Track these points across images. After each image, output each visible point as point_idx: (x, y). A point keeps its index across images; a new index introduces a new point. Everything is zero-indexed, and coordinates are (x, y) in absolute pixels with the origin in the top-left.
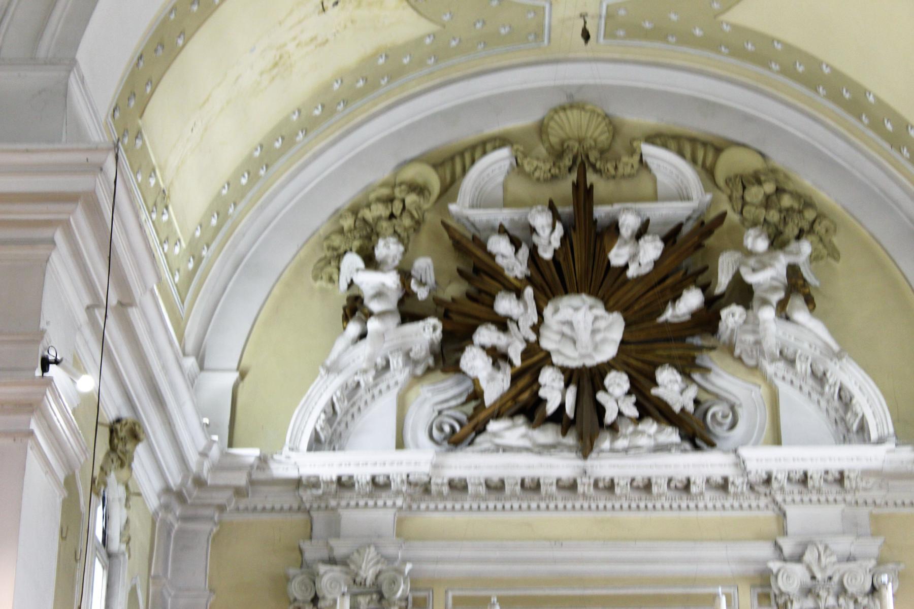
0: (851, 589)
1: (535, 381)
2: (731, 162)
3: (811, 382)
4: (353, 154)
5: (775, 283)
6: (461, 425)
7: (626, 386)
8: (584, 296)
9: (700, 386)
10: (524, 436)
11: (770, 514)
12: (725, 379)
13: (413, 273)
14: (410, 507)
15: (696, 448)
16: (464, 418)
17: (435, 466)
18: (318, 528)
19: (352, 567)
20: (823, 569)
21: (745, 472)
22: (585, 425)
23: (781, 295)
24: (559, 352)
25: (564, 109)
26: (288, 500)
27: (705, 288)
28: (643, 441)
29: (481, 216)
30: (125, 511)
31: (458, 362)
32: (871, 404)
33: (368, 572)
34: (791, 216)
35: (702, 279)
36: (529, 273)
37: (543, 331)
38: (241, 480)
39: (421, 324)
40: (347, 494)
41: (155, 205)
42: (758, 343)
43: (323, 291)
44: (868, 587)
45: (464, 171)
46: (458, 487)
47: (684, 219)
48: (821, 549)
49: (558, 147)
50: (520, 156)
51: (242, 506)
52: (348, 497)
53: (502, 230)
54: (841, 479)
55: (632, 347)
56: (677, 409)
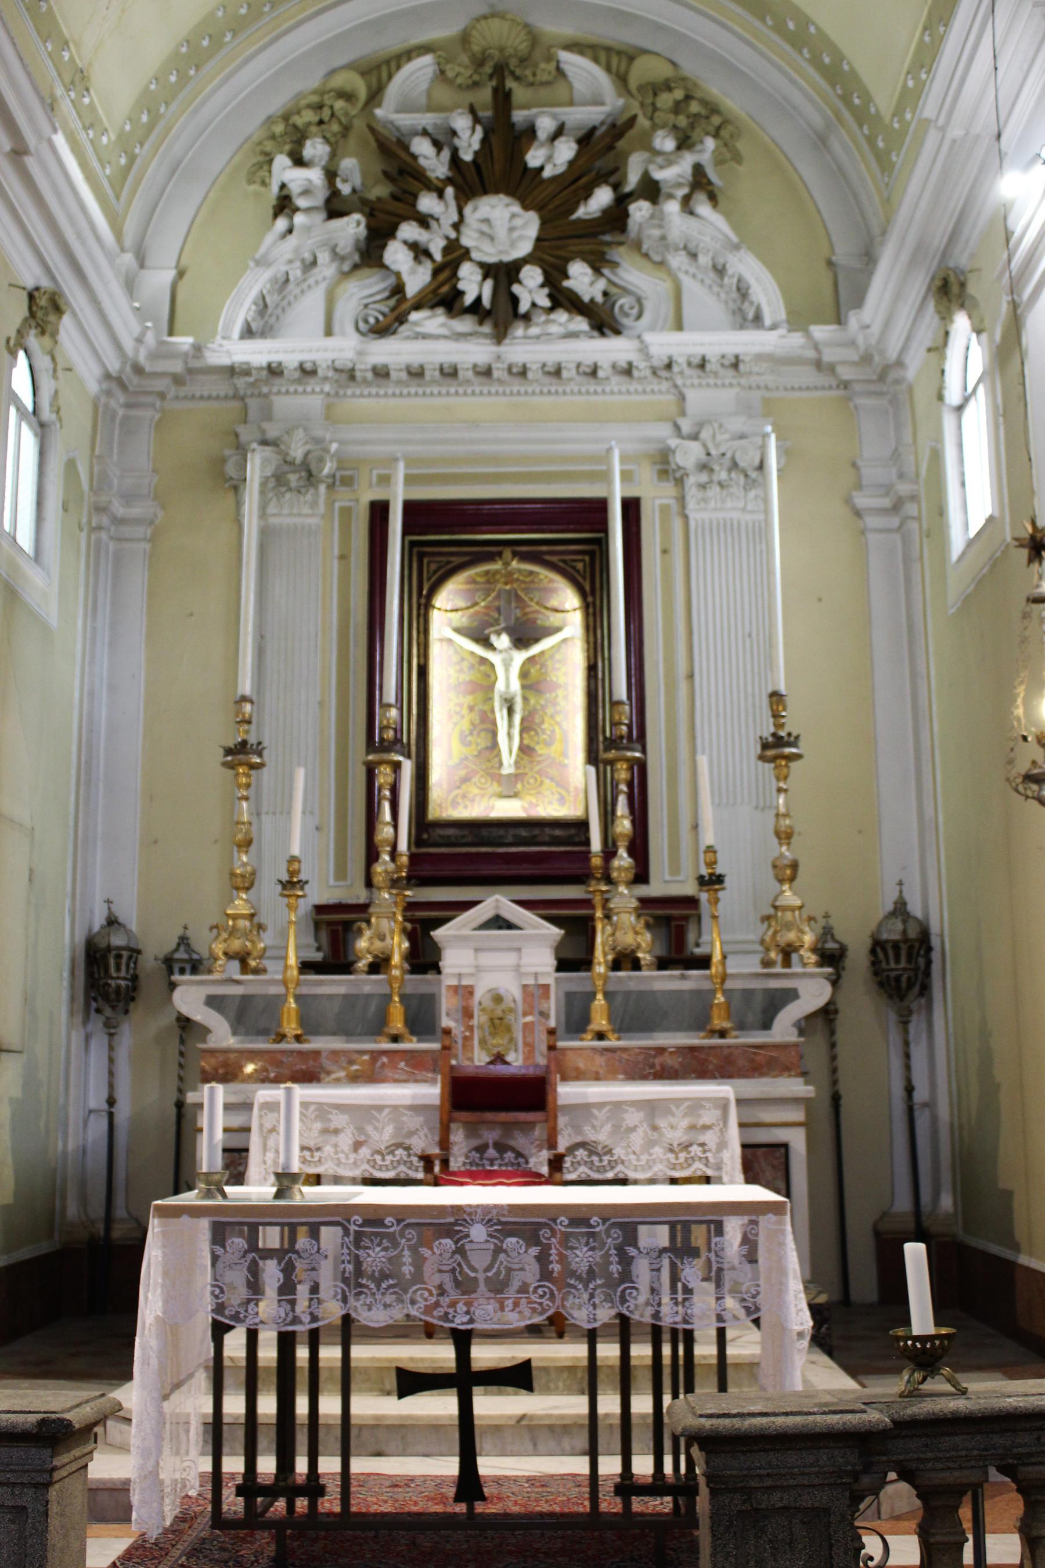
0: (742, 464)
1: (454, 276)
2: (643, 70)
3: (712, 275)
4: (283, 63)
5: (681, 180)
6: (384, 315)
7: (540, 279)
8: (502, 196)
9: (610, 281)
10: (443, 325)
11: (671, 398)
12: (632, 274)
13: (340, 172)
14: (337, 394)
15: (603, 334)
16: (386, 310)
17: (360, 353)
18: (253, 413)
19: (282, 447)
20: (717, 446)
21: (648, 357)
22: (501, 315)
23: (685, 191)
24: (478, 249)
25: (485, 17)
26: (223, 388)
27: (616, 187)
28: (554, 329)
29: (406, 120)
30: (53, 381)
31: (381, 257)
32: (767, 294)
33: (297, 453)
34: (695, 117)
35: (613, 179)
36: (450, 174)
37: (464, 229)
38: (177, 367)
39: (345, 219)
40: (278, 381)
41: (72, 83)
42: (663, 238)
43: (257, 194)
44: (757, 462)
45: (390, 77)
46: (381, 373)
47: (597, 123)
48: (716, 425)
49: (479, 56)
50: (442, 61)
51: (181, 394)
52: (278, 384)
53: (425, 133)
54: (736, 364)
55: (546, 244)
56: (586, 299)
